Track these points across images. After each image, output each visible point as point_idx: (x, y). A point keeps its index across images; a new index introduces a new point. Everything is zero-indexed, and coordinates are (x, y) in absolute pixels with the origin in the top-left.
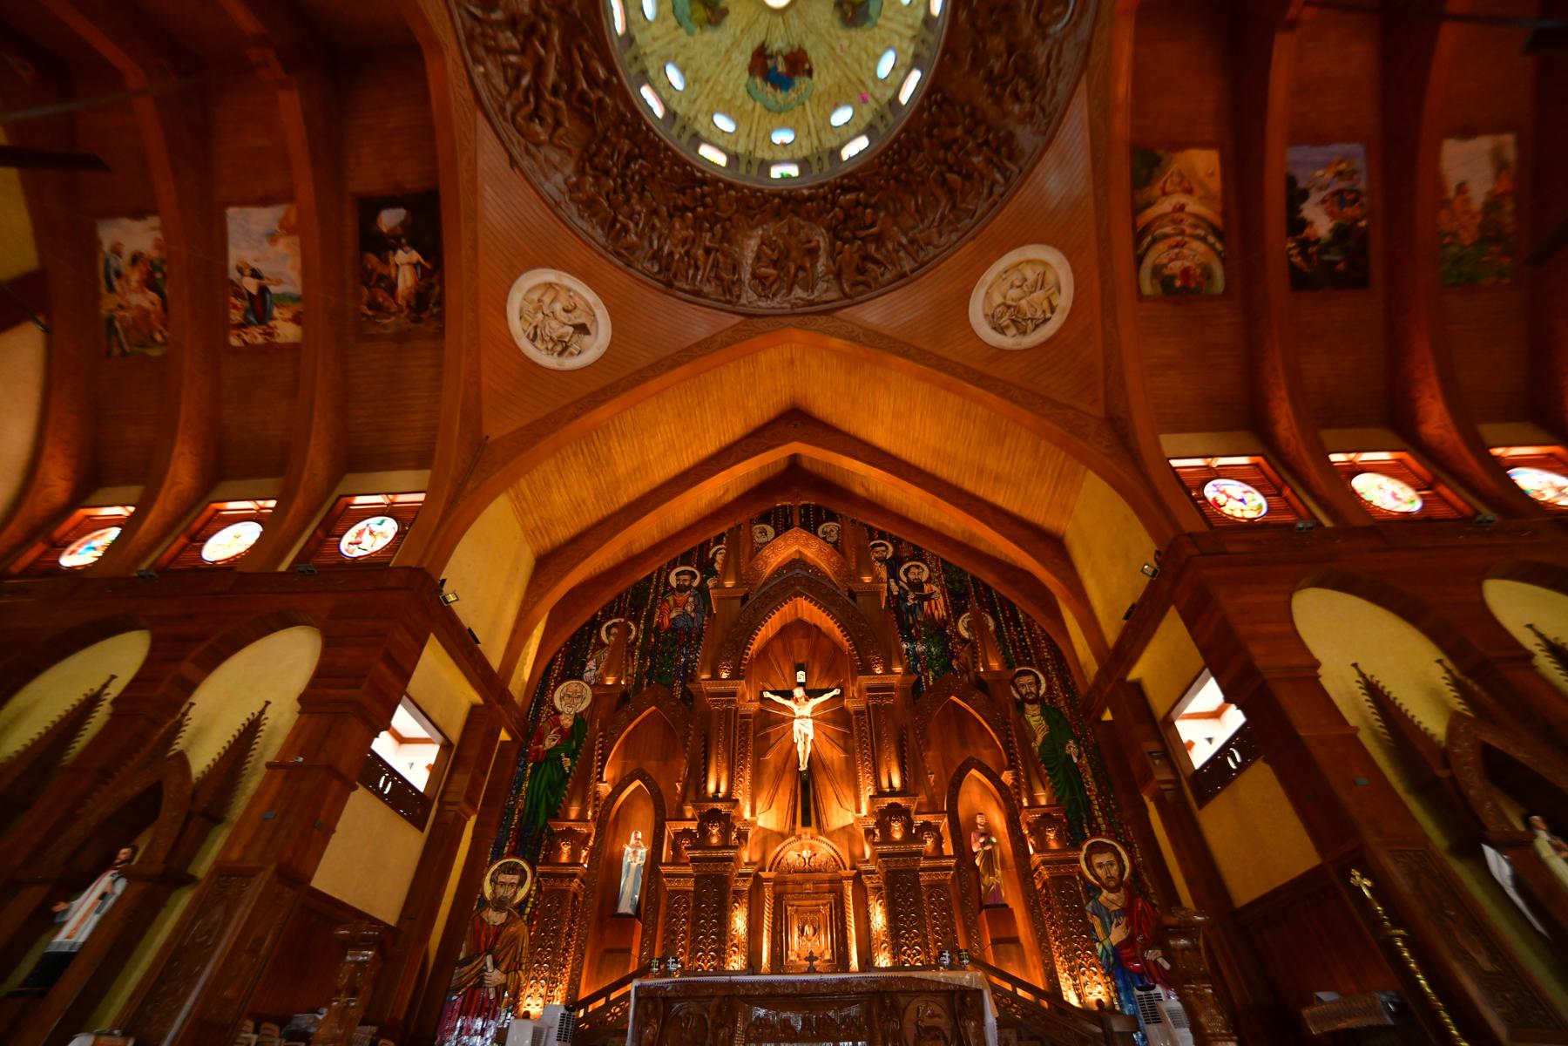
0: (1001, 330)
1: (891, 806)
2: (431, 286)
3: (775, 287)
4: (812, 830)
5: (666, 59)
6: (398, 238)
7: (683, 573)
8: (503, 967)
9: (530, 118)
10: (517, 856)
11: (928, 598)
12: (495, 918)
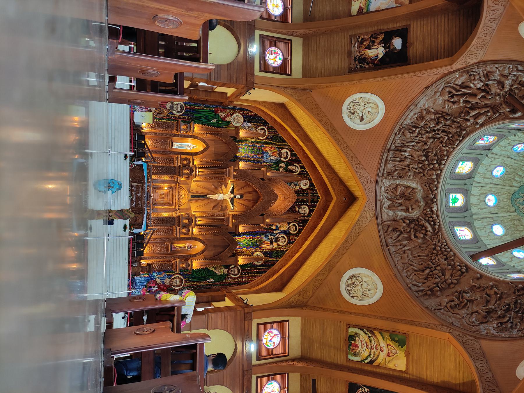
0: (351, 277)
2: (368, 64)
4: (190, 198)
6: (389, 47)
7: (287, 154)
9: (450, 92)
10: (186, 109)
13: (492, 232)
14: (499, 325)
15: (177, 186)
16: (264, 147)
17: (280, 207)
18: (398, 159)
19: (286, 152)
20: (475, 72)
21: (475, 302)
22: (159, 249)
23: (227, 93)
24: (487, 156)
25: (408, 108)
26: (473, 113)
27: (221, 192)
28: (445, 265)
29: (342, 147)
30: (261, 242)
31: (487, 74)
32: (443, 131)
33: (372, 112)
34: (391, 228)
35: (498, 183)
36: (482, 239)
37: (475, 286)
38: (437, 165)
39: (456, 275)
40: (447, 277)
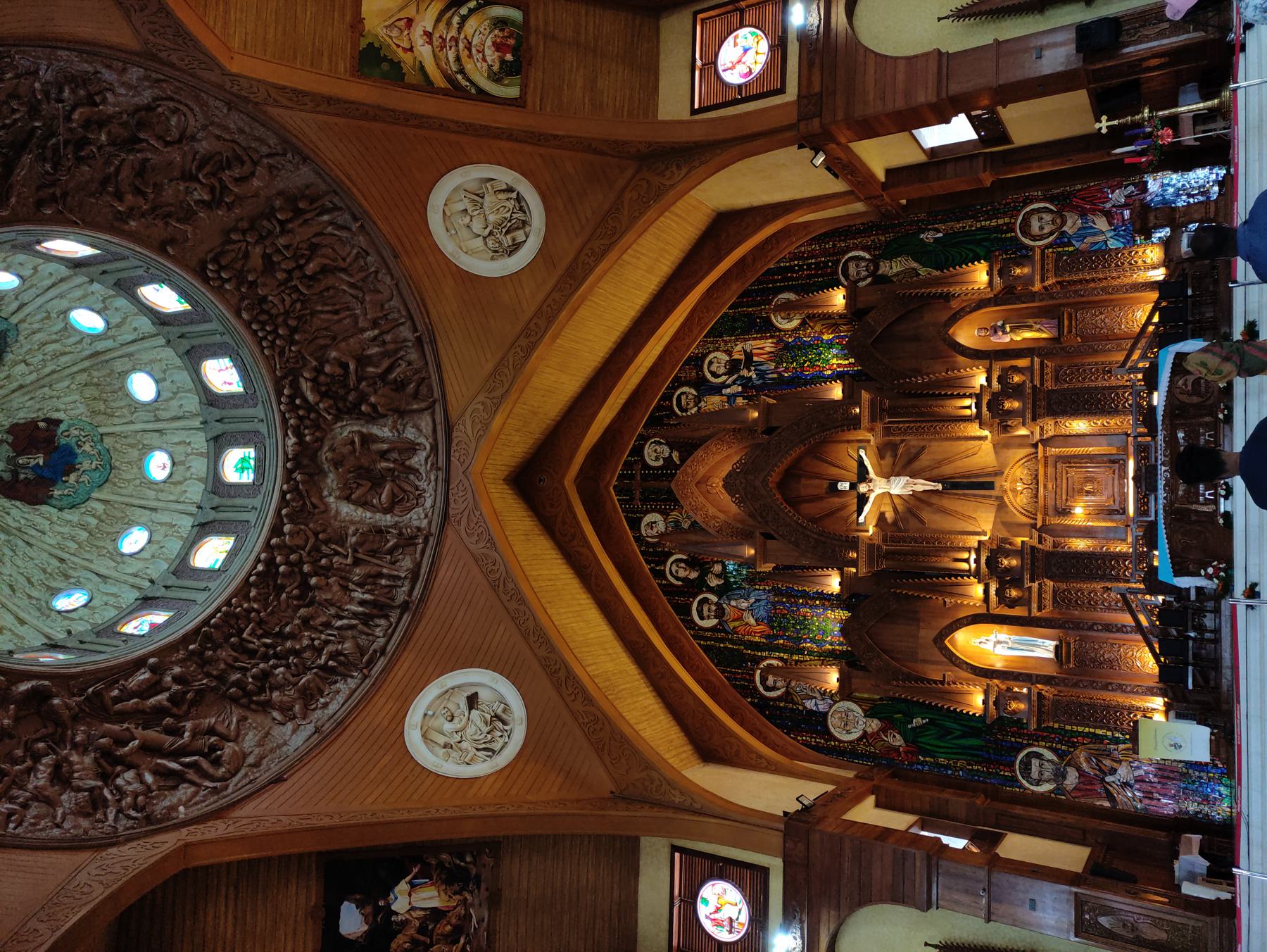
0: (516, 247)
1: (989, 409)
2: (441, 864)
3: (409, 488)
4: (998, 482)
5: (46, 610)
6: (377, 910)
8: (1115, 765)
11: (749, 356)
12: (1072, 778)
13: (157, 382)
14: (98, 99)
15: (1040, 517)
16: (767, 637)
17: (718, 457)
18: (383, 582)
19: (702, 618)
20: (129, 817)
21: (176, 174)
22: (1103, 320)
23: (878, 805)
24: (152, 581)
25: (341, 725)
26: (162, 697)
27: (897, 501)
28: (264, 285)
29: (531, 624)
30: (777, 357)
31: (95, 809)
32: (252, 653)
33: (442, 720)
34: (413, 390)
35: (138, 511)
36: (178, 362)
37: (178, 221)
38: (279, 559)
39: (233, 254)
40: (258, 250)
